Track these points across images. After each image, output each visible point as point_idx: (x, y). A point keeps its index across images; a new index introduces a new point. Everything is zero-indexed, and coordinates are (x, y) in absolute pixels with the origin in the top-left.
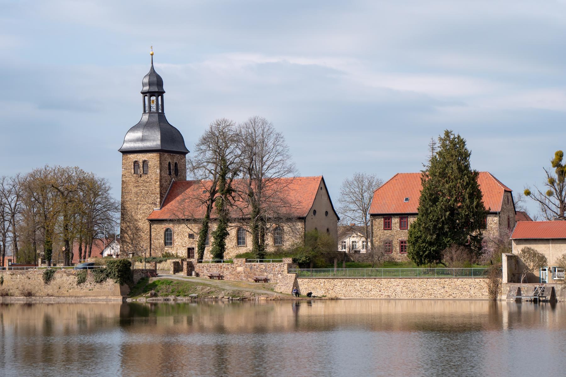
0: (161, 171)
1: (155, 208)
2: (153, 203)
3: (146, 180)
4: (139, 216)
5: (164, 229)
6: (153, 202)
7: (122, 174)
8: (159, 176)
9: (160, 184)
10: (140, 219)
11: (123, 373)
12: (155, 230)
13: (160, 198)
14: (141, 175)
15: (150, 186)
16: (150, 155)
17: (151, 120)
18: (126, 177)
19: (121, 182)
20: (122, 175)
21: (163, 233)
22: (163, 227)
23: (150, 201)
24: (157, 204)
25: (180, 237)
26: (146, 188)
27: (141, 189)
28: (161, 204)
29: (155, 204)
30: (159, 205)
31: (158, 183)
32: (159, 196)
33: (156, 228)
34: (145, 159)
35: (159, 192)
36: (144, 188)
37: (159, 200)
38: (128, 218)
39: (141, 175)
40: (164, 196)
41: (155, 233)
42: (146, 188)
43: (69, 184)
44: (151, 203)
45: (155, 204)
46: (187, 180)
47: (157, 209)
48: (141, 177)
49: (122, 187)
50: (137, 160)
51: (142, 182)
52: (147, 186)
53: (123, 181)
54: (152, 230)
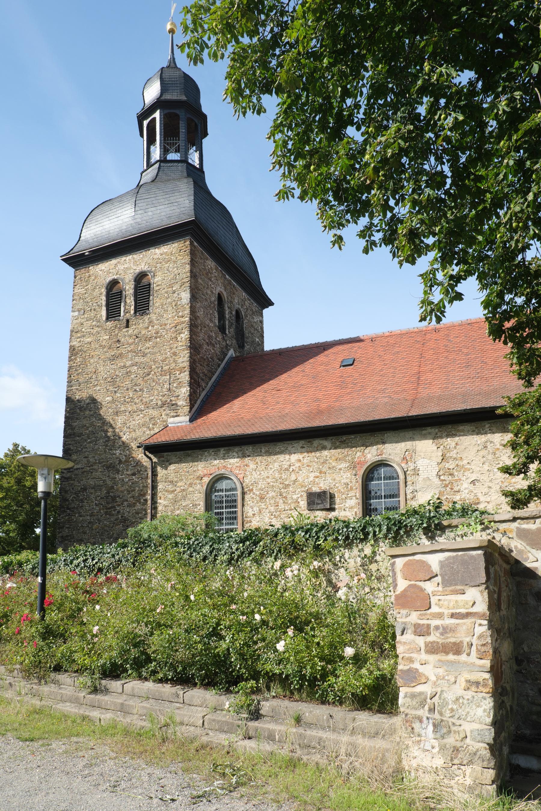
0: (194, 298)
1: (171, 420)
2: (163, 405)
3: (143, 332)
4: (118, 452)
5: (206, 480)
6: (164, 399)
7: (69, 328)
8: (187, 311)
9: (191, 339)
10: (120, 462)
11: (248, 92)
12: (170, 487)
13: (191, 385)
14: (128, 321)
15: (156, 350)
16: (157, 251)
17: (168, 97)
18: (84, 336)
19: (67, 354)
20: (72, 331)
21: (203, 496)
22: (200, 473)
23: (156, 399)
24: (180, 403)
25: (272, 509)
26: (142, 360)
27: (129, 363)
28: (191, 409)
29: (173, 406)
30: (187, 409)
31: (185, 335)
32: (185, 377)
33: (172, 477)
34: (143, 267)
35: (187, 364)
36: (137, 359)
37: (185, 391)
38: (85, 460)
39: (128, 321)
40: (203, 385)
41: (170, 496)
42: (142, 360)
43: (200, 646)
44: (160, 403)
45: (173, 406)
46: (268, 347)
47: (183, 420)
48: (127, 326)
49: (70, 368)
50: (116, 277)
51: (131, 341)
52: (147, 351)
53: (72, 349)
54: (160, 486)
